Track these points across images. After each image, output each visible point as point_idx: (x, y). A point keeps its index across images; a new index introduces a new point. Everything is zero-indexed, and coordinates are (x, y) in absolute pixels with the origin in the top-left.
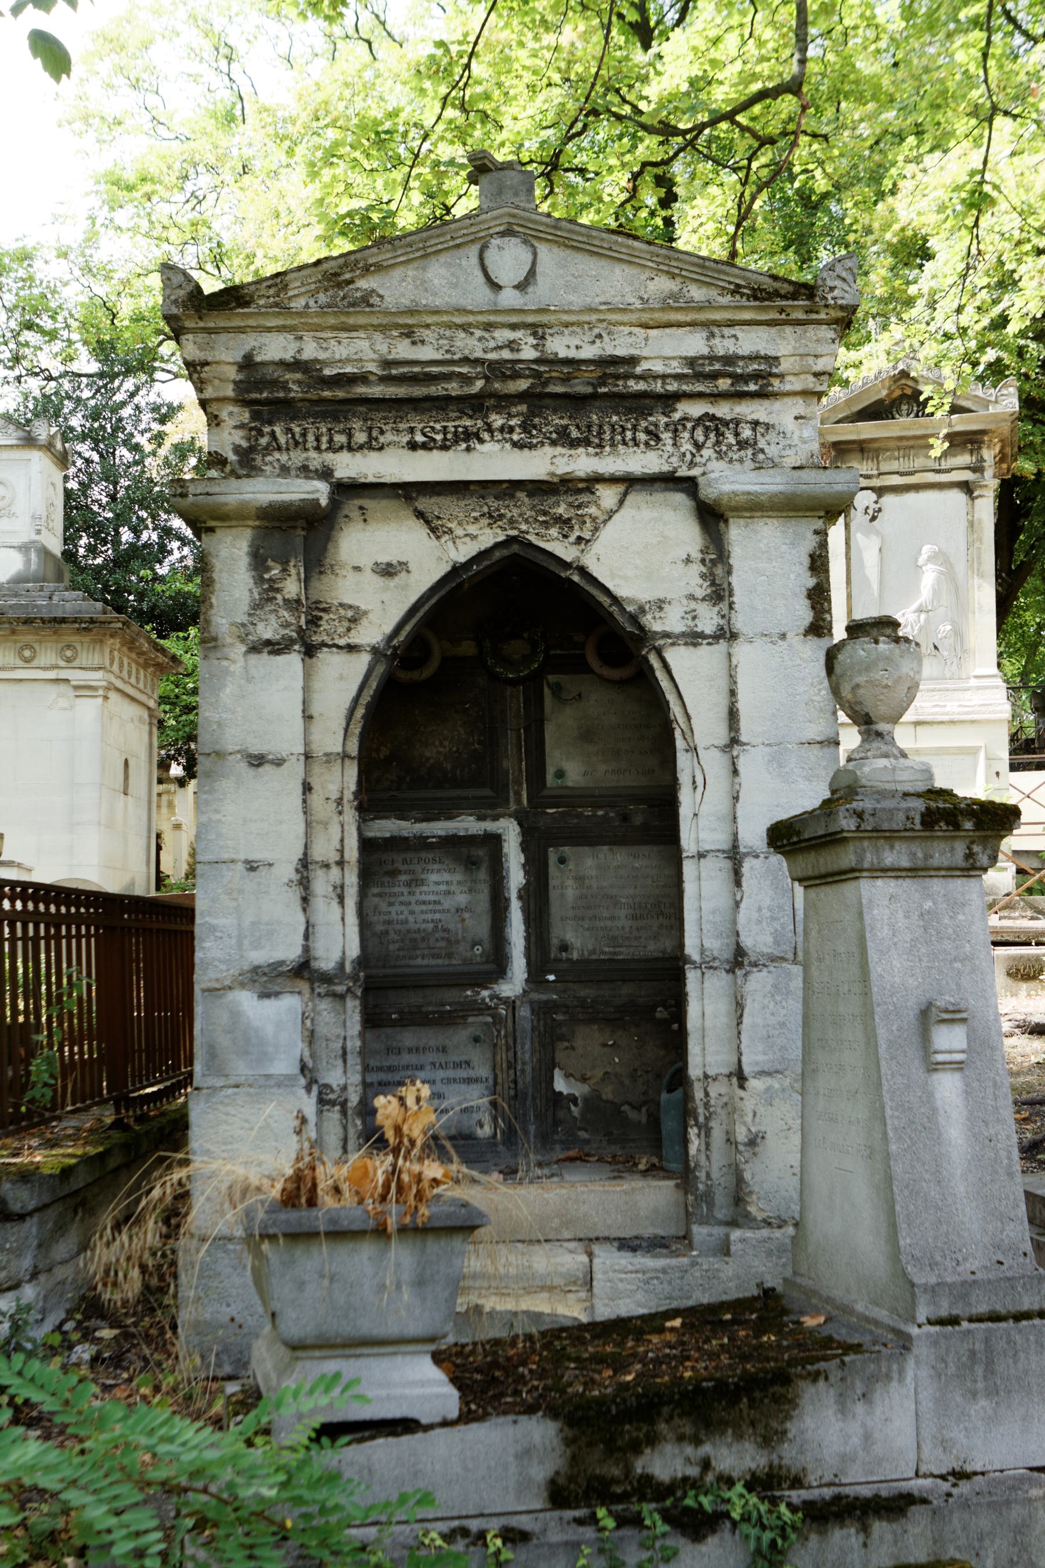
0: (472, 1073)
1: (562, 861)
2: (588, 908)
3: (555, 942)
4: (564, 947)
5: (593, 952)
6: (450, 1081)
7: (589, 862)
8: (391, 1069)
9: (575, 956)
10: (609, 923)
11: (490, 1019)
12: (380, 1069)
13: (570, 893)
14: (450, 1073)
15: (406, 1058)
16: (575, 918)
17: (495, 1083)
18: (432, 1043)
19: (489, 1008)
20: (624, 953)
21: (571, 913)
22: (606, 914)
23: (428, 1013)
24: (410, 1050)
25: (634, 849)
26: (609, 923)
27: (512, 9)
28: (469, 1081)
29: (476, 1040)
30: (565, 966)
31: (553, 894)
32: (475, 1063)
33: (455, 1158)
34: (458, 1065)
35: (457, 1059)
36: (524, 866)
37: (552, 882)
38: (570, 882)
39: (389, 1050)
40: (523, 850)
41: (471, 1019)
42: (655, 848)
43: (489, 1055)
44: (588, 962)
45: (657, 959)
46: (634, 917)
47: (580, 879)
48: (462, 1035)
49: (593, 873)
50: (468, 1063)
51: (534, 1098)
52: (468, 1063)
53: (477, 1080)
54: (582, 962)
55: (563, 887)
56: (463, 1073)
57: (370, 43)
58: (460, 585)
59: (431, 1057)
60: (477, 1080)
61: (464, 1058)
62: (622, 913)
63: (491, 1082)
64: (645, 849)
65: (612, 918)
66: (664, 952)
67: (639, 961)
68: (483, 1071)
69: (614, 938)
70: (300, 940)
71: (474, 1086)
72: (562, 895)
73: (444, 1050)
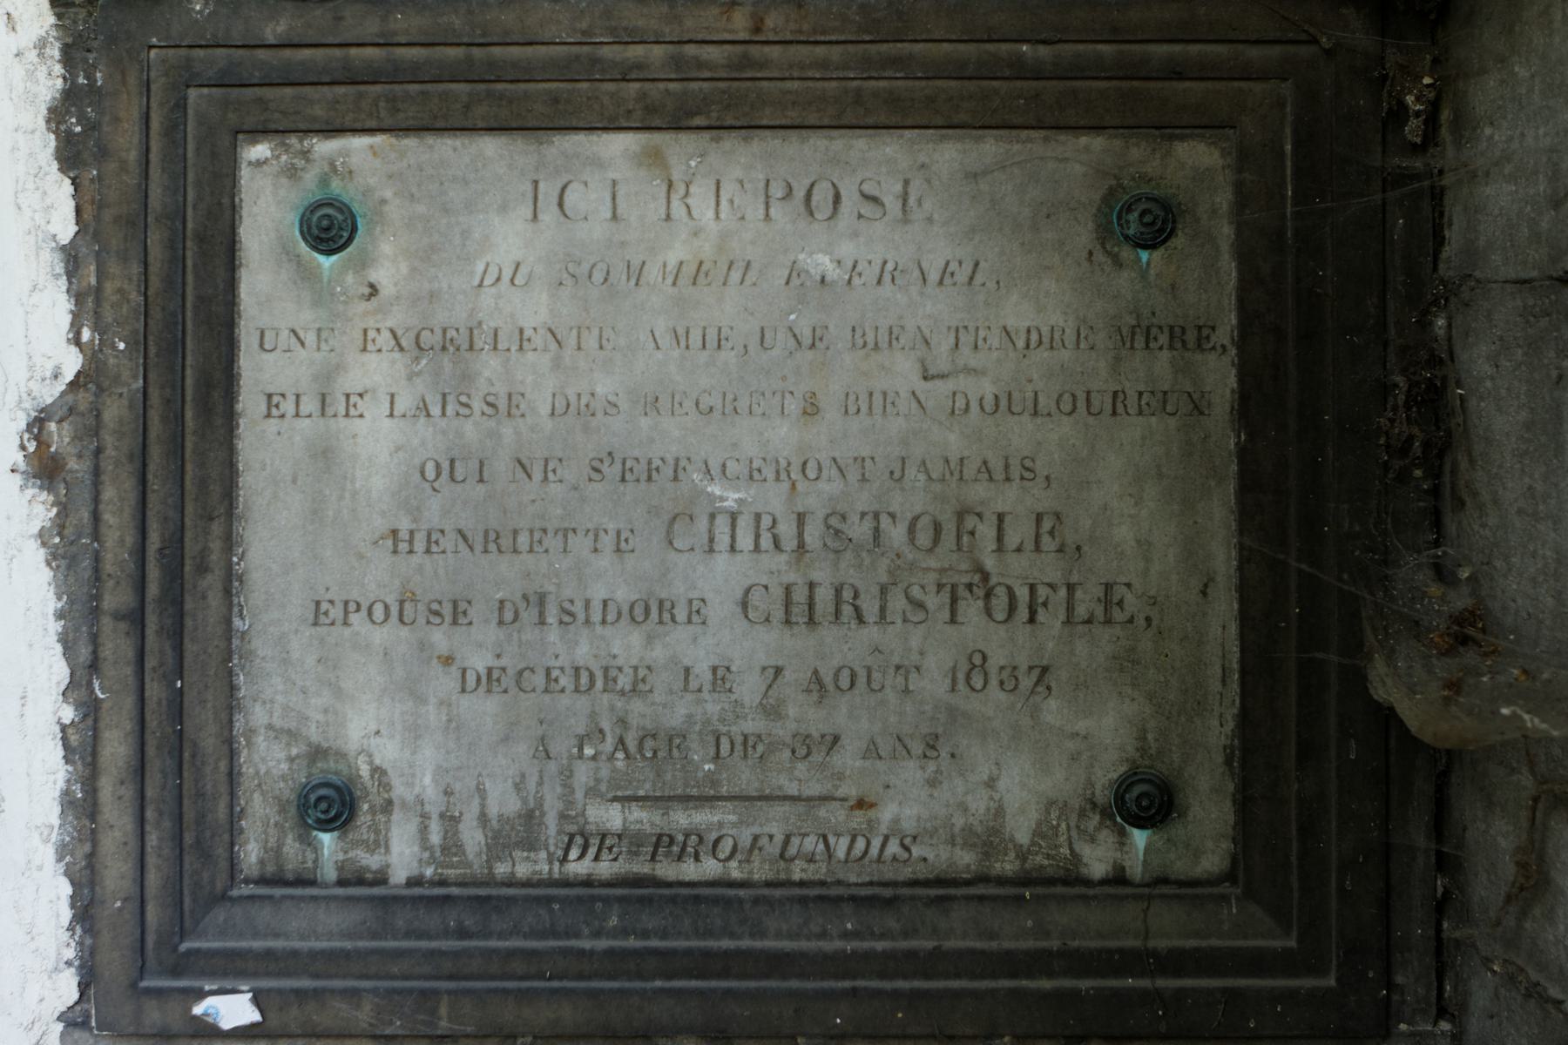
1: (330, 228)
2: (493, 541)
3: (269, 762)
4: (332, 802)
5: (522, 831)
7: (509, 239)
9: (401, 855)
10: (626, 645)
13: (380, 443)
16: (401, 610)
20: (729, 844)
21: (378, 577)
22: (610, 581)
25: (802, 157)
26: (626, 645)
27: (788, 819)
30: (320, 927)
31: (266, 449)
33: (1295, 934)
36: (71, 257)
37: (260, 371)
38: (376, 371)
40: (70, 157)
42: (948, 155)
44: (485, 900)
45: (942, 888)
46: (797, 610)
47: (444, 350)
49: (534, 309)
54: (454, 900)
55: (328, 399)
57: (561, 205)
62: (719, 577)
64: (879, 160)
65: (653, 611)
66: (989, 840)
67: (822, 898)
69: (662, 745)
72: (324, 455)
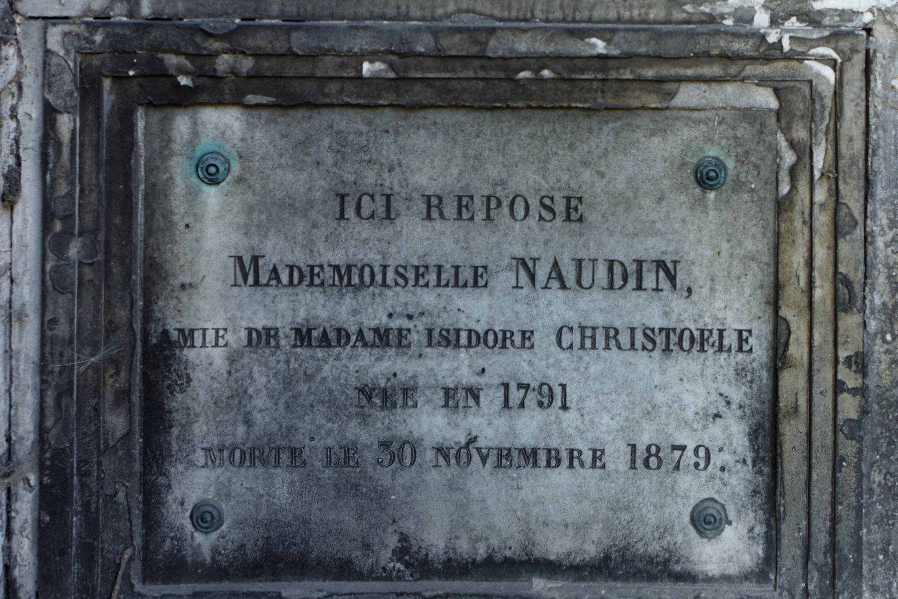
0: (682, 313)
6: (589, 337)
8: (348, 278)
11: (766, 99)
12: (306, 276)
14: (595, 307)
15: (417, 238)
17: (778, 359)
18: (527, 180)
19: (770, 53)
23: (510, 64)
24: (432, 206)
28: (668, 341)
29: (706, 178)
32: (694, 272)
34: (626, 276)
35: (623, 251)
39: (345, 202)
41: (688, 95)
43: (757, 243)
48: (648, 155)
50: (667, 269)
51: (90, 49)
52: (667, 269)
53: (700, 341)
56: (648, 310)
58: (110, 131)
59: (519, 237)
60: (700, 341)
61: (652, 248)
63: (760, 349)
68: (731, 304)
70: (233, 278)
71: (686, 364)
73: (573, 211)
